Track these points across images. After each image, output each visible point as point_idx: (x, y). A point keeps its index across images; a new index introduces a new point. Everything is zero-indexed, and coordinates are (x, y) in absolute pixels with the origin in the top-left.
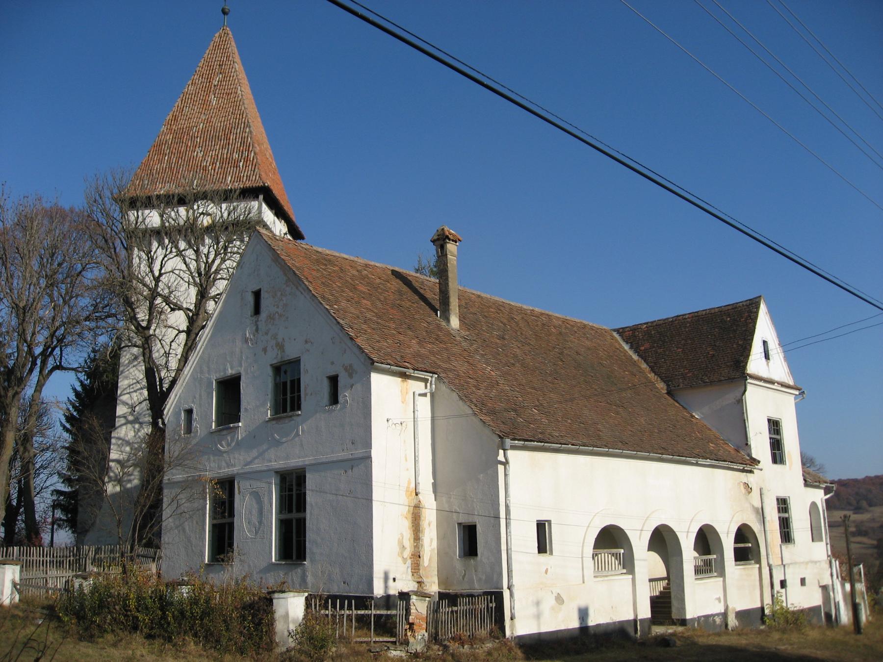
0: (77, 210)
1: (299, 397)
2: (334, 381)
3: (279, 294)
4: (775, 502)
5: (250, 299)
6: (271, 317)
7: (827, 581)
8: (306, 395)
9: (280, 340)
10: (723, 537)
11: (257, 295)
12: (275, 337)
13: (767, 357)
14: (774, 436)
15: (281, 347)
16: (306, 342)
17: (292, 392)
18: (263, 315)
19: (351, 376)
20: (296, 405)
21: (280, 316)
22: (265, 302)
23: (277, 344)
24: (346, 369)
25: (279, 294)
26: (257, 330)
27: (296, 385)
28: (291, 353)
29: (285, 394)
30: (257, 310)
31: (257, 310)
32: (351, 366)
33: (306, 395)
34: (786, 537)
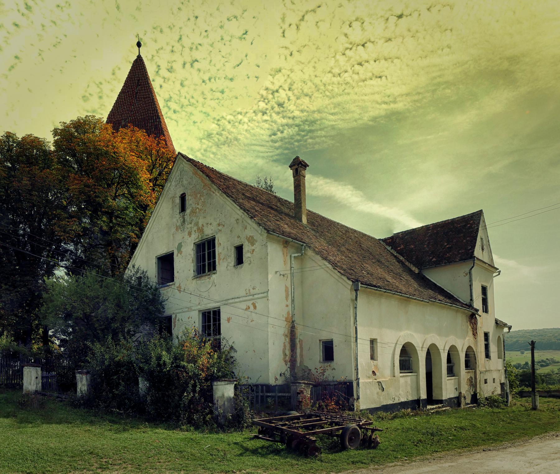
0: (60, 128)
1: (214, 262)
2: (239, 250)
3: (199, 195)
4: (483, 335)
5: (178, 201)
6: (193, 212)
7: (503, 381)
8: (219, 259)
9: (200, 226)
10: (419, 352)
11: (183, 198)
12: (197, 224)
13: (483, 249)
14: (212, 313)
15: (201, 230)
16: (219, 225)
17: (209, 259)
18: (188, 211)
19: (253, 244)
20: (213, 267)
21: (200, 210)
22: (189, 201)
23: (198, 229)
24: (249, 240)
25: (199, 195)
26: (184, 221)
27: (212, 255)
28: (209, 232)
29: (204, 261)
30: (183, 209)
31: (183, 209)
32: (252, 237)
33: (219, 259)
34: (488, 356)
